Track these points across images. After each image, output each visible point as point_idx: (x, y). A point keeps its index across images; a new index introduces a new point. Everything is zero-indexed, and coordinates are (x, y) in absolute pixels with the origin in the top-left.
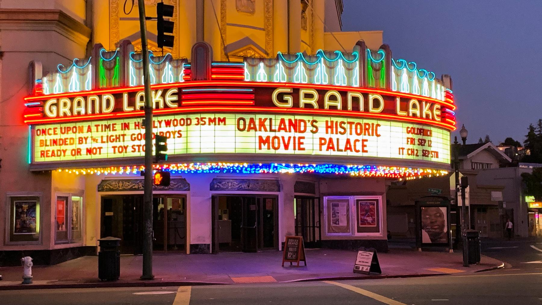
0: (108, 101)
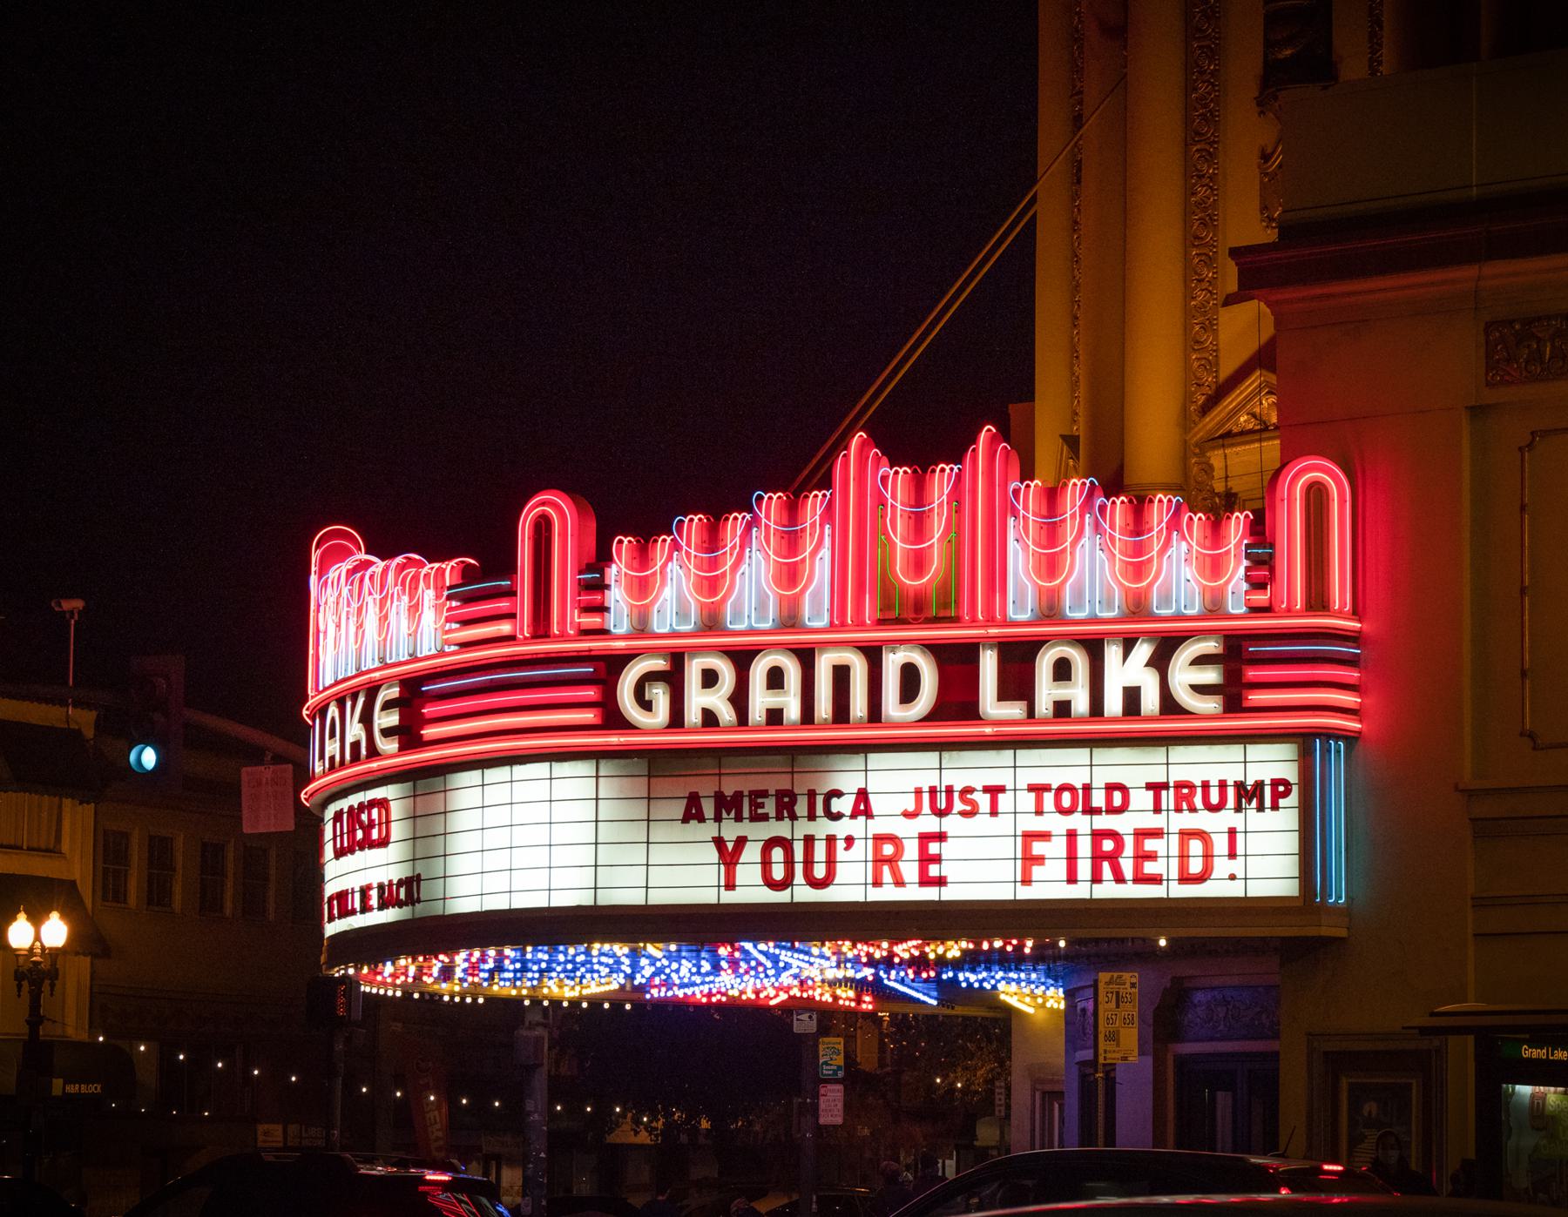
0: (910, 678)
